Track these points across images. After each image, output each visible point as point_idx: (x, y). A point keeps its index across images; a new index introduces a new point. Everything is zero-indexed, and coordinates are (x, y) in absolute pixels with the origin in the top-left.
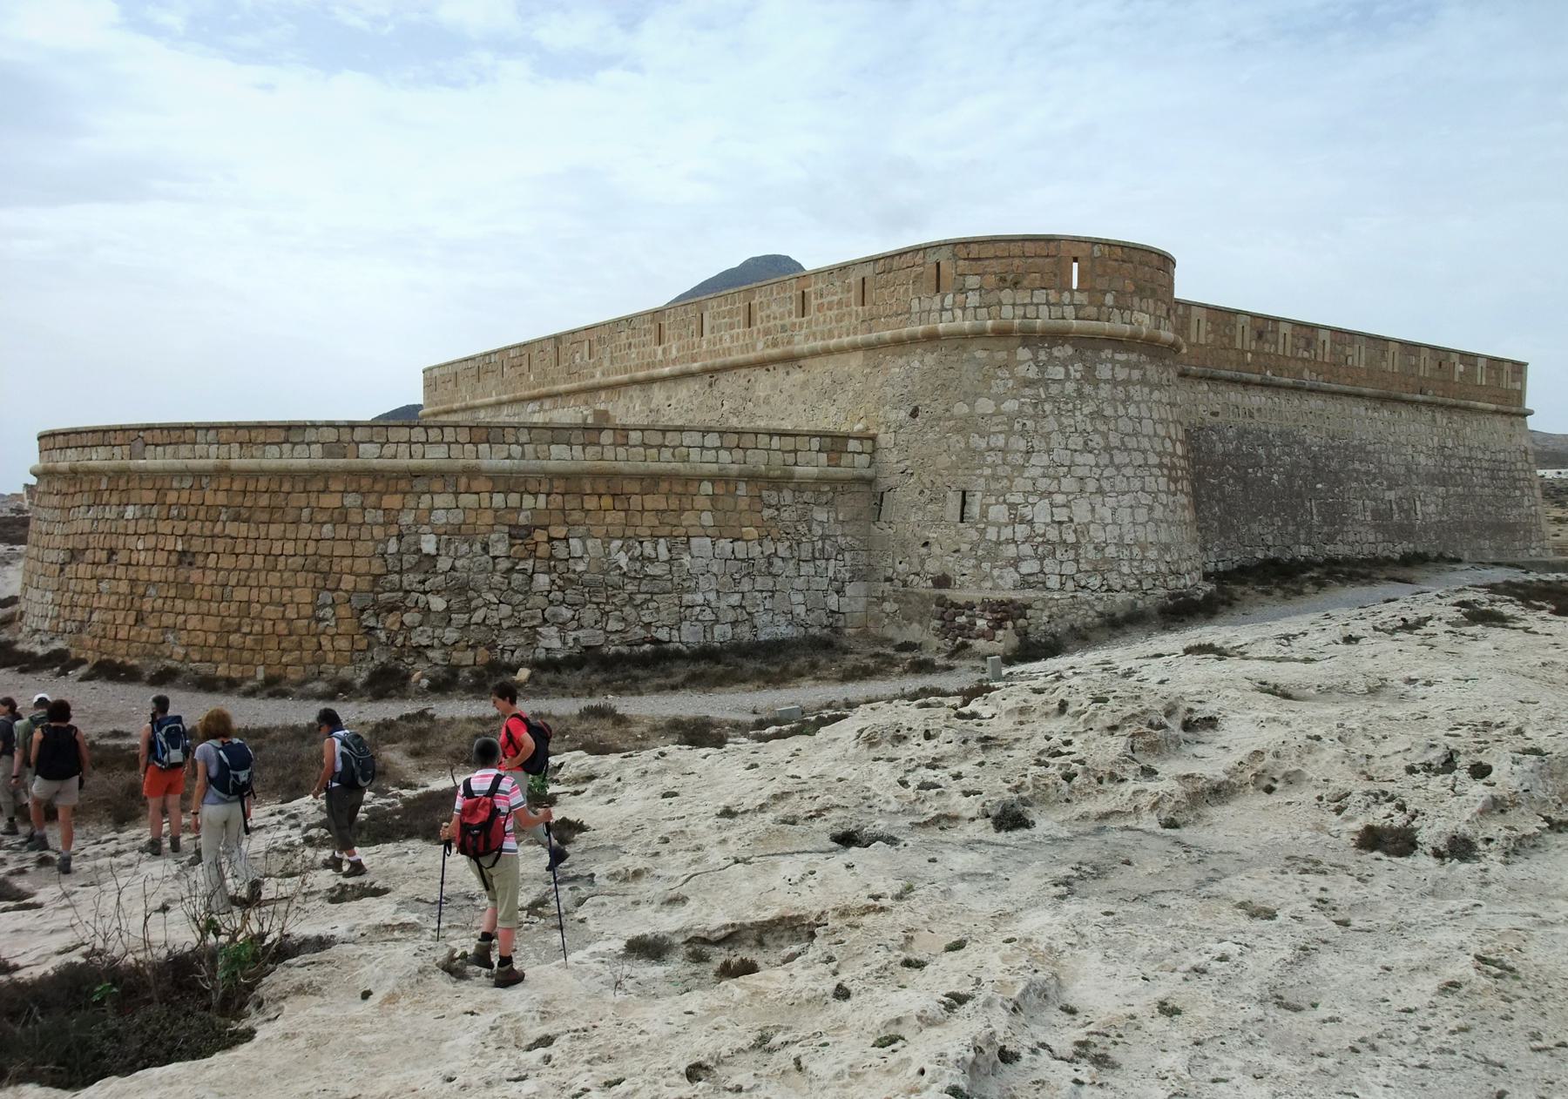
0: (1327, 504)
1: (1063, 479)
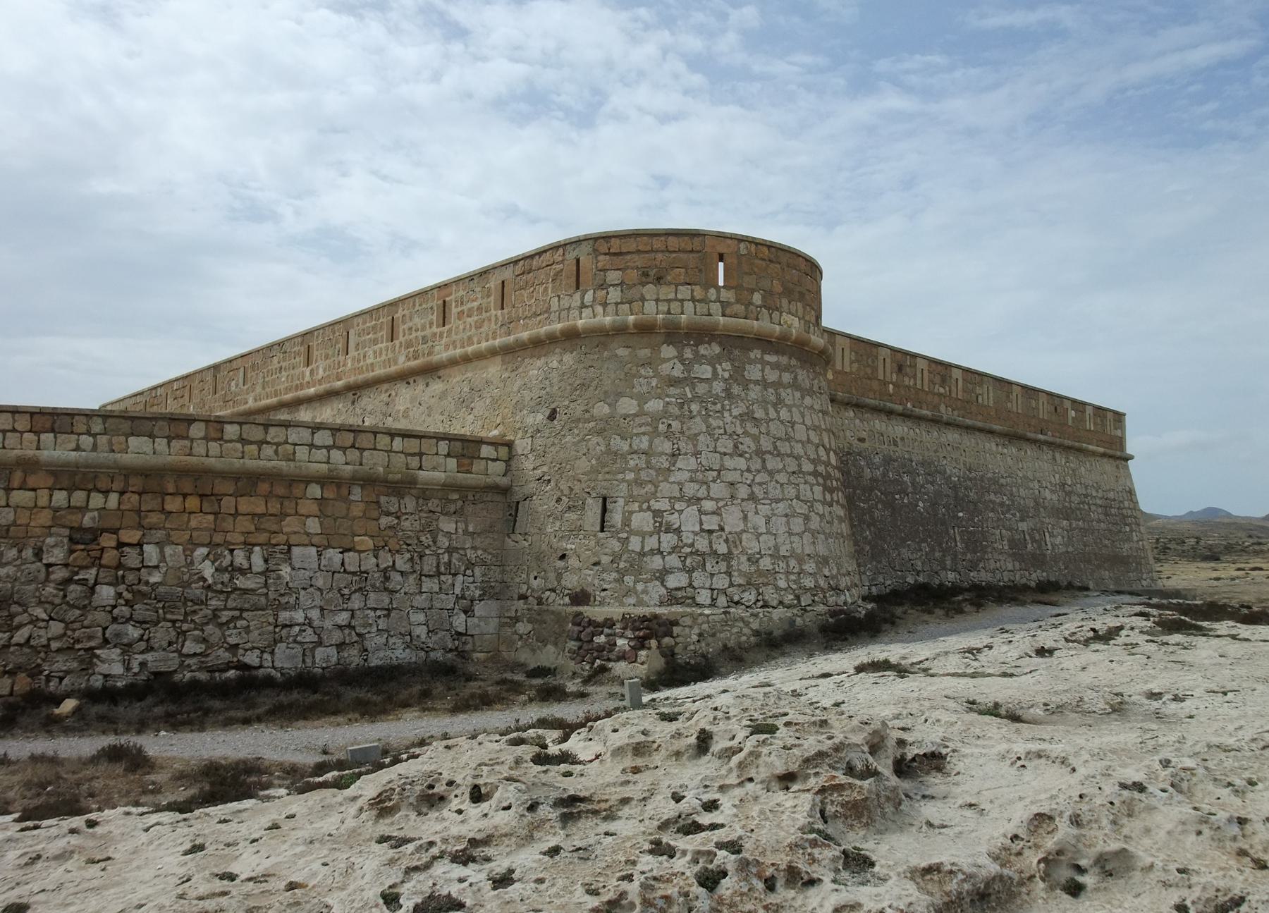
0: (968, 532)
1: (712, 485)
